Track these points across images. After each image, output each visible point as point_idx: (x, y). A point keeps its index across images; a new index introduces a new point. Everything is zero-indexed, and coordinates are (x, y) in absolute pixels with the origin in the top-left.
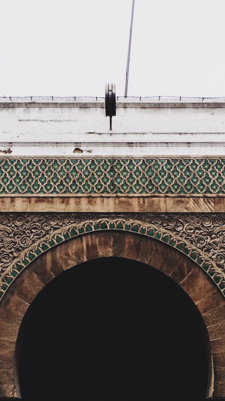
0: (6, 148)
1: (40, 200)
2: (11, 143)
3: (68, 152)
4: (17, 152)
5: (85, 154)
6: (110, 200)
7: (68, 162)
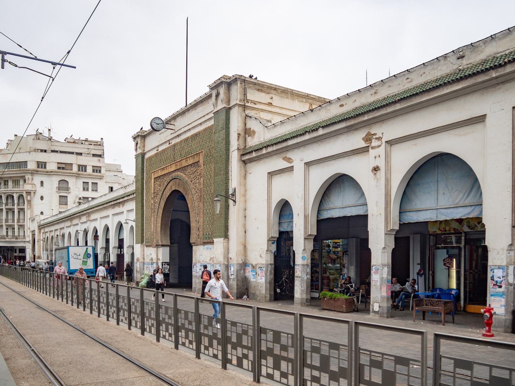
0: (157, 149)
1: (163, 169)
2: (158, 146)
3: (167, 146)
4: (161, 149)
5: (171, 144)
6: (174, 165)
7: (168, 148)
